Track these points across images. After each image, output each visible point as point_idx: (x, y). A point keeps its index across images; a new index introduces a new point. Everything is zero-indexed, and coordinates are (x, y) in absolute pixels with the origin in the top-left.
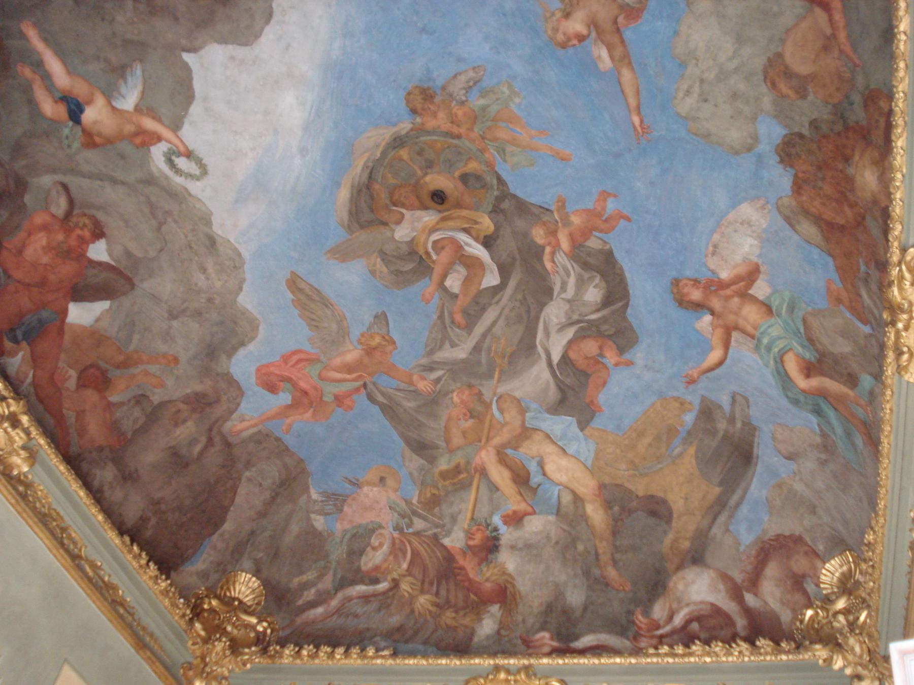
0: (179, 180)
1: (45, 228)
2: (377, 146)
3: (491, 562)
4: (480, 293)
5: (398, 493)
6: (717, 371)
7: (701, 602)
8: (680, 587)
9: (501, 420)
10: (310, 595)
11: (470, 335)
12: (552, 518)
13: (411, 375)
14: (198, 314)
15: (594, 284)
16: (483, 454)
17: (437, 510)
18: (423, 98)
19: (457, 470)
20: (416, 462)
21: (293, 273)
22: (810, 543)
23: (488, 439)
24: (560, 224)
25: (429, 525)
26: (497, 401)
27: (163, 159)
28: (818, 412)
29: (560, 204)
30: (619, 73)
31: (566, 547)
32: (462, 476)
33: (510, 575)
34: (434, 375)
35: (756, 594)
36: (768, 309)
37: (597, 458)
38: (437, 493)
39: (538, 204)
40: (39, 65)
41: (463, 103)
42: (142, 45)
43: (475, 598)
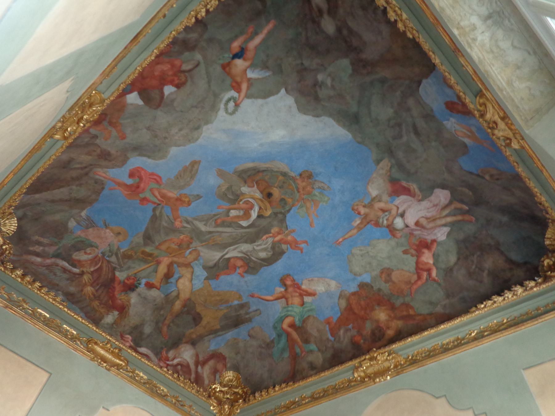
0: (222, 106)
1: (173, 66)
2: (279, 168)
5: (119, 243)
6: (266, 302)
7: (185, 360)
8: (183, 349)
9: (186, 255)
10: (39, 249)
12: (163, 296)
13: (179, 217)
14: (156, 136)
16: (166, 259)
17: (126, 260)
18: (307, 176)
19: (150, 255)
20: (140, 240)
23: (174, 256)
27: (230, 97)
28: (279, 336)
30: (354, 229)
31: (158, 308)
32: (150, 258)
33: (130, 304)
34: (185, 225)
36: (303, 304)
37: (198, 291)
40: (256, 33)
41: (313, 188)
42: (281, 72)
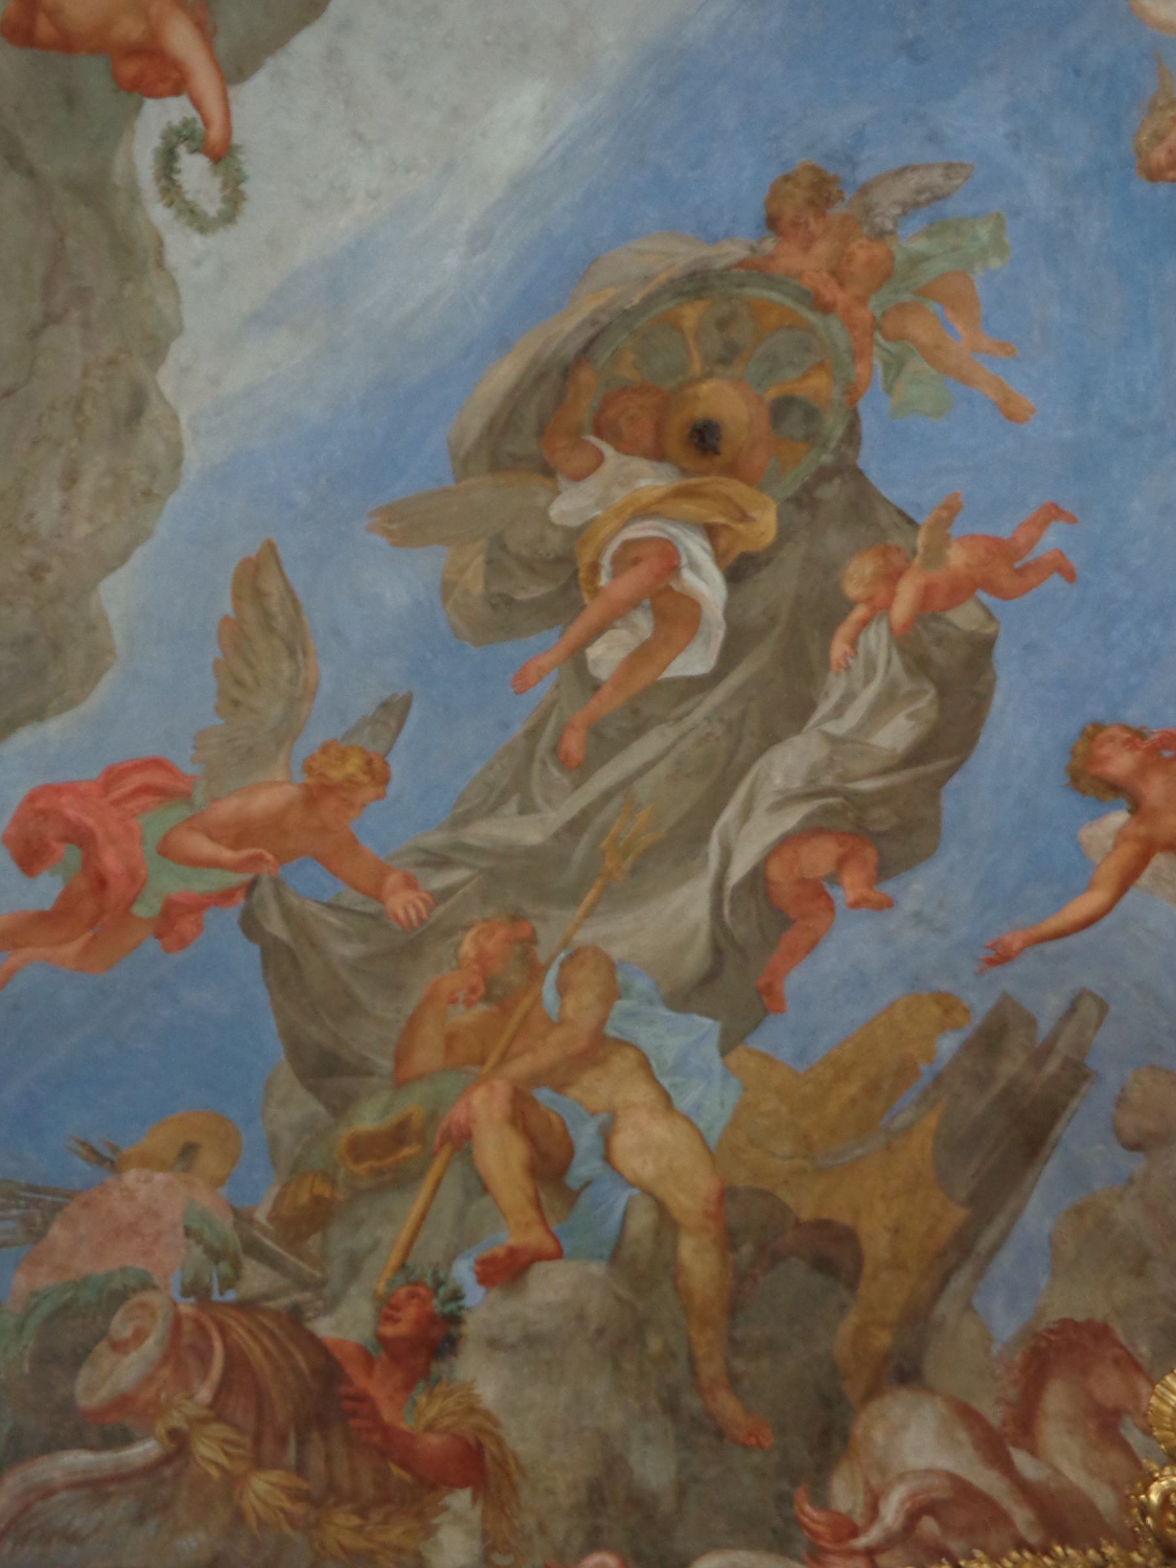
0: (159, 214)
2: (646, 279)
3: (438, 1380)
4: (657, 687)
5: (223, 1191)
8: (879, 1436)
11: (577, 787)
12: (597, 1269)
13: (382, 872)
15: (912, 709)
16: (478, 1097)
17: (314, 1242)
19: (399, 1135)
20: (305, 1106)
21: (270, 548)
22: (1123, 1340)
23: (505, 1058)
24: (917, 561)
25: (283, 1282)
26: (562, 965)
27: (156, 142)
29: (945, 514)
31: (621, 1341)
32: (407, 1151)
33: (487, 1414)
34: (440, 881)
35: (1033, 1452)
38: (327, 1194)
39: (901, 505)
41: (881, 235)
43: (407, 1477)
